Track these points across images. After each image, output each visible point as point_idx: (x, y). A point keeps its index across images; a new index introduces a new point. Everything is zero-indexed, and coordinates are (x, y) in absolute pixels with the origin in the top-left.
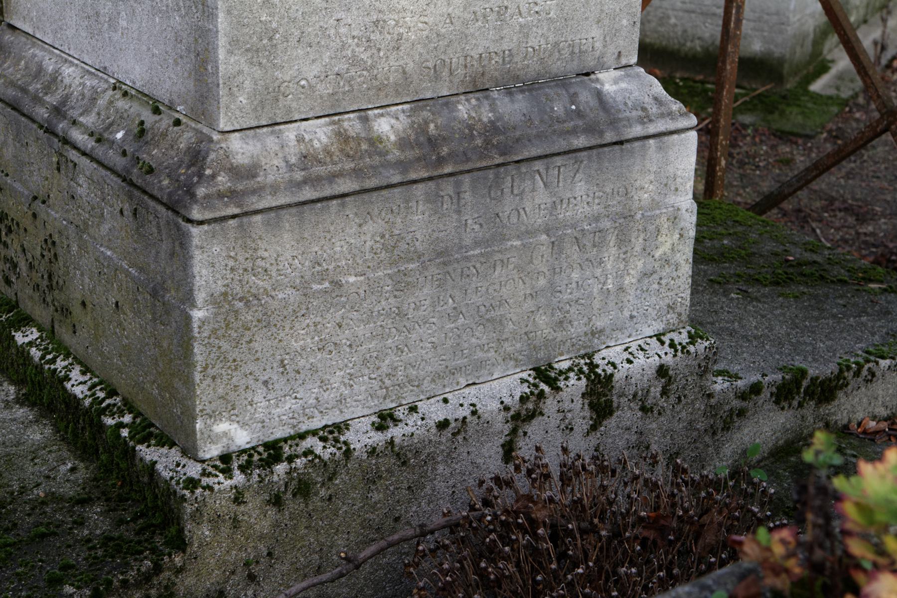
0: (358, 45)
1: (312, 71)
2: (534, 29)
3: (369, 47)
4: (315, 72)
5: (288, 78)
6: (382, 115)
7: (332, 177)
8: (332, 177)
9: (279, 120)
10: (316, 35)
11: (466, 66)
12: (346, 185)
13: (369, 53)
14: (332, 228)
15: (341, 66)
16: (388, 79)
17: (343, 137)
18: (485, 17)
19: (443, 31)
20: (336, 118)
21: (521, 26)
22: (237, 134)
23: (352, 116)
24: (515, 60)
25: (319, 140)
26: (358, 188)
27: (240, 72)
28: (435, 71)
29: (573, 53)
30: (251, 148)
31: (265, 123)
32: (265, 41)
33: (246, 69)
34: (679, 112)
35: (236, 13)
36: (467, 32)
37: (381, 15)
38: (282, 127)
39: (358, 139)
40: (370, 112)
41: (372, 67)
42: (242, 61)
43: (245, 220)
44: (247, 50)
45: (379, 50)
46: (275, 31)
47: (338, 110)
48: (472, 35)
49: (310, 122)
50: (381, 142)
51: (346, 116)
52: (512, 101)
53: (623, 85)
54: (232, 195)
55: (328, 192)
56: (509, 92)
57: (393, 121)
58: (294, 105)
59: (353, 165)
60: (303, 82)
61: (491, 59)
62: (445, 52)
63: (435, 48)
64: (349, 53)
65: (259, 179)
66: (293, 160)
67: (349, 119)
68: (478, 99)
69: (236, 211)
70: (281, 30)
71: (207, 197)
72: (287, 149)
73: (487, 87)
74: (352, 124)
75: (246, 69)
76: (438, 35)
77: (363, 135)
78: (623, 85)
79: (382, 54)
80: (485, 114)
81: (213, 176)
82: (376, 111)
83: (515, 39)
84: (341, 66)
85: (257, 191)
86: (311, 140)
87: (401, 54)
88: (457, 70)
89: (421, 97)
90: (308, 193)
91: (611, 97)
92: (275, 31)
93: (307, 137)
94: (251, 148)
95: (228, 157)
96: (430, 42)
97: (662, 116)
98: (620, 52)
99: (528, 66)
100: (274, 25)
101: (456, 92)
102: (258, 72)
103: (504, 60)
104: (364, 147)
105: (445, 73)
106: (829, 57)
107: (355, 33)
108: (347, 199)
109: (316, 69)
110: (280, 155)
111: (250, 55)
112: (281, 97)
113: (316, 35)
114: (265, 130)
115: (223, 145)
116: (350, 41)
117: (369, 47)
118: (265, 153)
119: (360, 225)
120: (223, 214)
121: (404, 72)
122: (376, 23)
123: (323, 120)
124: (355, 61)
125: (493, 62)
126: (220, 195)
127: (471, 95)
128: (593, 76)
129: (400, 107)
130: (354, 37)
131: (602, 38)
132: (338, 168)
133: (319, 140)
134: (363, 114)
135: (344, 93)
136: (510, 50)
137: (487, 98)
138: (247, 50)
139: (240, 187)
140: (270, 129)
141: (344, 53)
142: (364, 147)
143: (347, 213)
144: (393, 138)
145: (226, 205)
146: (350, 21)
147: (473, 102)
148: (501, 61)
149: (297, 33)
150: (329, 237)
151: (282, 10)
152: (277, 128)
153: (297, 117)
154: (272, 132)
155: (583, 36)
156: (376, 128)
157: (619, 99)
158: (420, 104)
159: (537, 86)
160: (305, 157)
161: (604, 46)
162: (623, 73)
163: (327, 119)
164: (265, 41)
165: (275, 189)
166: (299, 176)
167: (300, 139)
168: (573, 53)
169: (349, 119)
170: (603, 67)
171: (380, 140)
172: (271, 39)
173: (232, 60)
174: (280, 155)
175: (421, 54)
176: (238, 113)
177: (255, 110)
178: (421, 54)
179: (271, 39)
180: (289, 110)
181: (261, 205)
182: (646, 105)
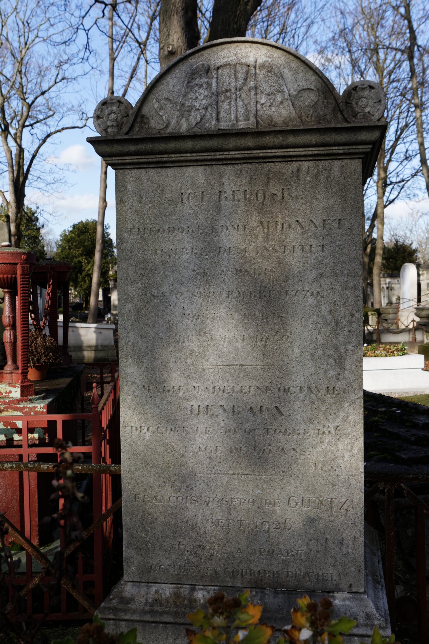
0: (190, 555)
1: (166, 563)
2: (292, 563)
3: (196, 556)
4: (168, 563)
5: (155, 563)
6: (203, 589)
7: (162, 613)
8: (162, 613)
9: (151, 581)
10: (168, 547)
11: (251, 574)
12: (167, 618)
13: (196, 559)
14: (160, 637)
15: (182, 563)
16: (207, 573)
17: (177, 595)
18: (260, 552)
19: (236, 555)
20: (179, 586)
21: (283, 560)
22: (131, 583)
23: (187, 586)
24: (281, 576)
25: (165, 595)
26: (173, 621)
27: (132, 557)
28: (233, 574)
29: (318, 579)
30: (133, 591)
31: (144, 581)
32: (144, 546)
33: (135, 556)
34: (379, 626)
35: (130, 531)
36: (250, 558)
37: (201, 543)
38: (152, 584)
39: (184, 598)
40: (197, 587)
41: (198, 566)
42: (133, 552)
43: (118, 622)
44: (136, 548)
45: (201, 559)
46: (149, 542)
47: (181, 582)
48: (254, 560)
49: (166, 585)
50: (195, 602)
51: (184, 586)
52: (275, 597)
53: (348, 603)
54: (115, 610)
55: (158, 619)
56: (276, 593)
57: (205, 593)
58: (158, 576)
59: (175, 610)
60: (162, 567)
61: (265, 574)
62: (238, 566)
63: (232, 563)
64: (185, 557)
65: (129, 606)
66: (150, 600)
67: (186, 588)
68: (257, 592)
69: (114, 617)
70: (151, 542)
71: (104, 608)
72: (149, 595)
73: (264, 587)
74: (185, 591)
75: (135, 556)
76: (233, 557)
77: (187, 597)
78: (348, 603)
79: (203, 561)
80: (256, 601)
81: (112, 599)
82: (200, 587)
83: (280, 566)
84: (181, 563)
85: (125, 611)
86: (162, 593)
87: (213, 562)
88: (246, 575)
89: (225, 585)
90: (148, 618)
91: (338, 608)
92: (149, 542)
93: (160, 591)
94: (133, 591)
95: (122, 592)
96: (229, 560)
97: (366, 625)
98: (351, 585)
99: (289, 581)
100: (148, 539)
101: (245, 586)
102: (141, 559)
103: (274, 576)
104: (186, 602)
105: (239, 576)
106: (415, 310)
107: (188, 549)
108: (168, 625)
109: (168, 562)
110: (145, 597)
111: (137, 550)
112: (152, 571)
113: (168, 547)
114: (144, 584)
115: (123, 587)
116: (186, 552)
117: (196, 556)
118: (138, 594)
119: (175, 639)
120: (108, 617)
121: (216, 572)
122: (200, 546)
123: (172, 586)
124: (188, 562)
125: (267, 575)
126: (110, 608)
127: (254, 589)
128: (331, 594)
129: (213, 587)
130: (188, 551)
131: (337, 575)
132: (167, 609)
133: (165, 595)
134: (193, 587)
135: (183, 575)
136: (277, 571)
137: (262, 592)
138: (136, 548)
139: (119, 607)
140: (147, 584)
141: (183, 557)
142: (186, 602)
143: (168, 632)
144: (202, 601)
145: (109, 614)
146: (185, 543)
147: (254, 593)
148: (272, 576)
149: (159, 544)
150: (158, 640)
151: (152, 534)
152: (150, 584)
153: (159, 581)
154: (147, 586)
155: (324, 571)
156: (195, 595)
157: (342, 609)
158: (224, 588)
159: (294, 592)
160: (156, 600)
161: (340, 580)
162: (351, 596)
163: (175, 585)
164: (144, 546)
165: (134, 612)
166: (148, 608)
167: (157, 592)
168: (318, 579)
169: (186, 588)
170: (339, 590)
171: (195, 601)
172: (146, 545)
173: (129, 551)
174: (145, 597)
175: (224, 564)
176: (131, 574)
177: (139, 574)
178: (224, 564)
179: (146, 545)
180: (156, 578)
181: (126, 617)
182: (358, 617)
